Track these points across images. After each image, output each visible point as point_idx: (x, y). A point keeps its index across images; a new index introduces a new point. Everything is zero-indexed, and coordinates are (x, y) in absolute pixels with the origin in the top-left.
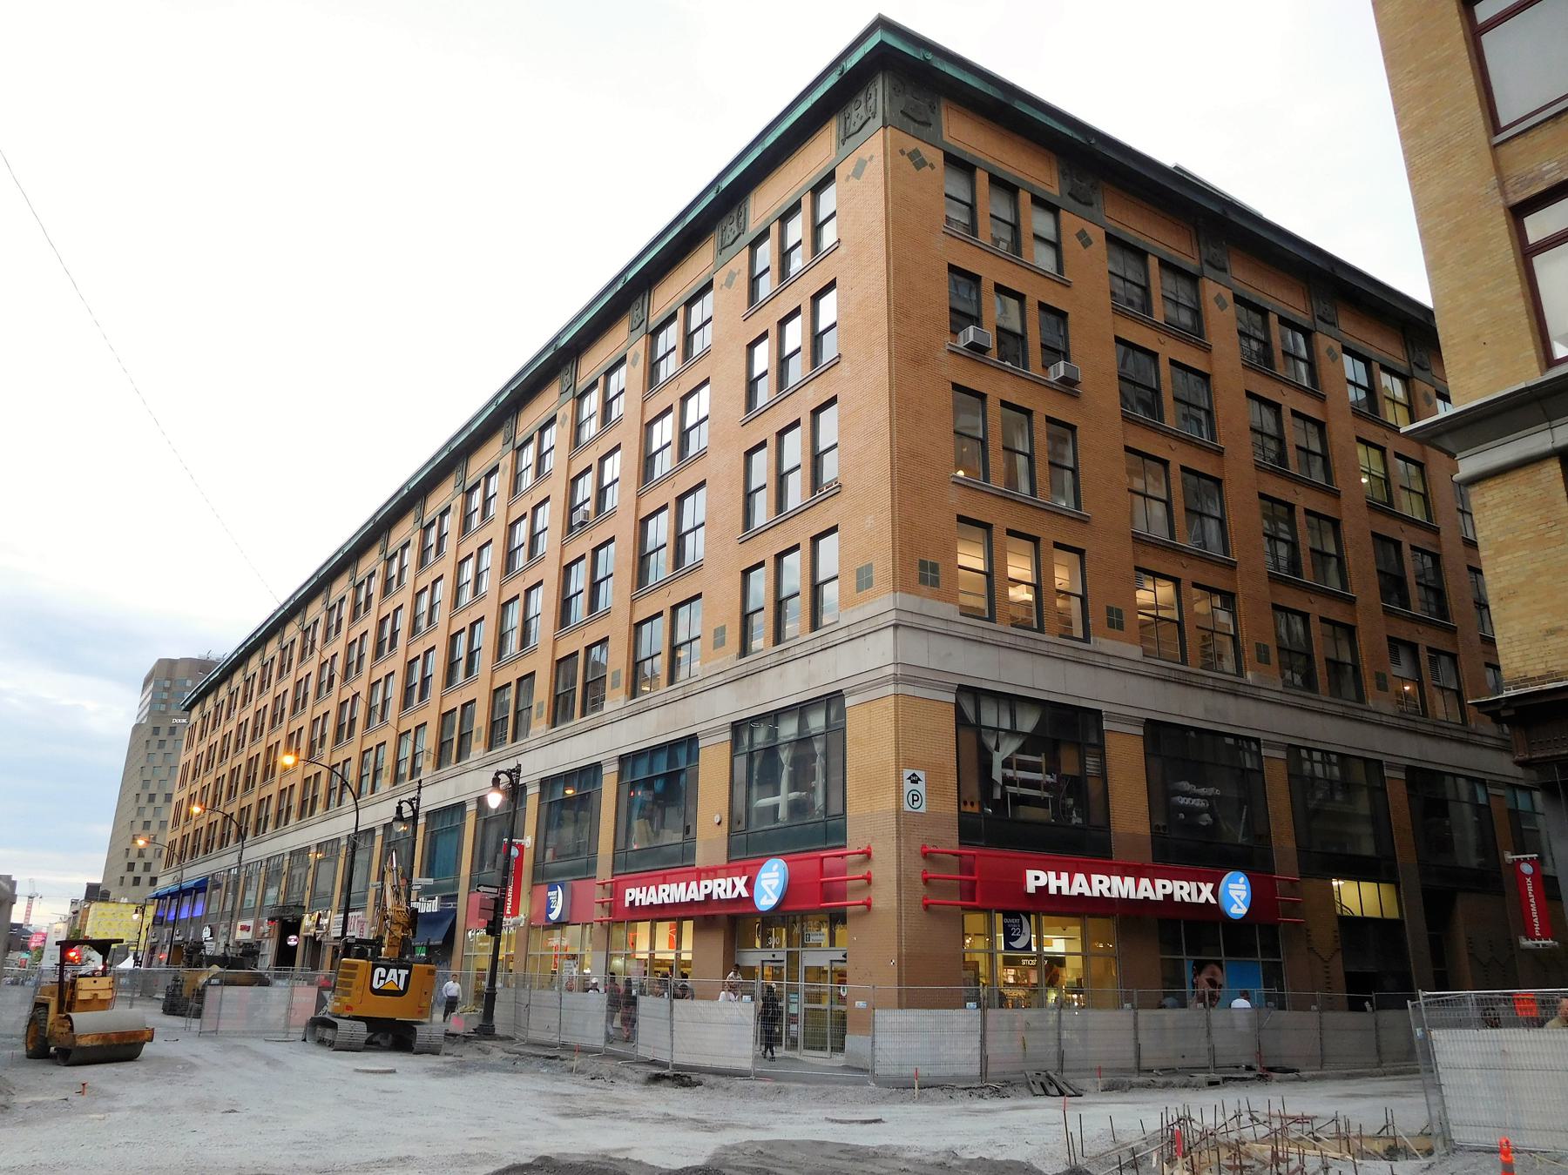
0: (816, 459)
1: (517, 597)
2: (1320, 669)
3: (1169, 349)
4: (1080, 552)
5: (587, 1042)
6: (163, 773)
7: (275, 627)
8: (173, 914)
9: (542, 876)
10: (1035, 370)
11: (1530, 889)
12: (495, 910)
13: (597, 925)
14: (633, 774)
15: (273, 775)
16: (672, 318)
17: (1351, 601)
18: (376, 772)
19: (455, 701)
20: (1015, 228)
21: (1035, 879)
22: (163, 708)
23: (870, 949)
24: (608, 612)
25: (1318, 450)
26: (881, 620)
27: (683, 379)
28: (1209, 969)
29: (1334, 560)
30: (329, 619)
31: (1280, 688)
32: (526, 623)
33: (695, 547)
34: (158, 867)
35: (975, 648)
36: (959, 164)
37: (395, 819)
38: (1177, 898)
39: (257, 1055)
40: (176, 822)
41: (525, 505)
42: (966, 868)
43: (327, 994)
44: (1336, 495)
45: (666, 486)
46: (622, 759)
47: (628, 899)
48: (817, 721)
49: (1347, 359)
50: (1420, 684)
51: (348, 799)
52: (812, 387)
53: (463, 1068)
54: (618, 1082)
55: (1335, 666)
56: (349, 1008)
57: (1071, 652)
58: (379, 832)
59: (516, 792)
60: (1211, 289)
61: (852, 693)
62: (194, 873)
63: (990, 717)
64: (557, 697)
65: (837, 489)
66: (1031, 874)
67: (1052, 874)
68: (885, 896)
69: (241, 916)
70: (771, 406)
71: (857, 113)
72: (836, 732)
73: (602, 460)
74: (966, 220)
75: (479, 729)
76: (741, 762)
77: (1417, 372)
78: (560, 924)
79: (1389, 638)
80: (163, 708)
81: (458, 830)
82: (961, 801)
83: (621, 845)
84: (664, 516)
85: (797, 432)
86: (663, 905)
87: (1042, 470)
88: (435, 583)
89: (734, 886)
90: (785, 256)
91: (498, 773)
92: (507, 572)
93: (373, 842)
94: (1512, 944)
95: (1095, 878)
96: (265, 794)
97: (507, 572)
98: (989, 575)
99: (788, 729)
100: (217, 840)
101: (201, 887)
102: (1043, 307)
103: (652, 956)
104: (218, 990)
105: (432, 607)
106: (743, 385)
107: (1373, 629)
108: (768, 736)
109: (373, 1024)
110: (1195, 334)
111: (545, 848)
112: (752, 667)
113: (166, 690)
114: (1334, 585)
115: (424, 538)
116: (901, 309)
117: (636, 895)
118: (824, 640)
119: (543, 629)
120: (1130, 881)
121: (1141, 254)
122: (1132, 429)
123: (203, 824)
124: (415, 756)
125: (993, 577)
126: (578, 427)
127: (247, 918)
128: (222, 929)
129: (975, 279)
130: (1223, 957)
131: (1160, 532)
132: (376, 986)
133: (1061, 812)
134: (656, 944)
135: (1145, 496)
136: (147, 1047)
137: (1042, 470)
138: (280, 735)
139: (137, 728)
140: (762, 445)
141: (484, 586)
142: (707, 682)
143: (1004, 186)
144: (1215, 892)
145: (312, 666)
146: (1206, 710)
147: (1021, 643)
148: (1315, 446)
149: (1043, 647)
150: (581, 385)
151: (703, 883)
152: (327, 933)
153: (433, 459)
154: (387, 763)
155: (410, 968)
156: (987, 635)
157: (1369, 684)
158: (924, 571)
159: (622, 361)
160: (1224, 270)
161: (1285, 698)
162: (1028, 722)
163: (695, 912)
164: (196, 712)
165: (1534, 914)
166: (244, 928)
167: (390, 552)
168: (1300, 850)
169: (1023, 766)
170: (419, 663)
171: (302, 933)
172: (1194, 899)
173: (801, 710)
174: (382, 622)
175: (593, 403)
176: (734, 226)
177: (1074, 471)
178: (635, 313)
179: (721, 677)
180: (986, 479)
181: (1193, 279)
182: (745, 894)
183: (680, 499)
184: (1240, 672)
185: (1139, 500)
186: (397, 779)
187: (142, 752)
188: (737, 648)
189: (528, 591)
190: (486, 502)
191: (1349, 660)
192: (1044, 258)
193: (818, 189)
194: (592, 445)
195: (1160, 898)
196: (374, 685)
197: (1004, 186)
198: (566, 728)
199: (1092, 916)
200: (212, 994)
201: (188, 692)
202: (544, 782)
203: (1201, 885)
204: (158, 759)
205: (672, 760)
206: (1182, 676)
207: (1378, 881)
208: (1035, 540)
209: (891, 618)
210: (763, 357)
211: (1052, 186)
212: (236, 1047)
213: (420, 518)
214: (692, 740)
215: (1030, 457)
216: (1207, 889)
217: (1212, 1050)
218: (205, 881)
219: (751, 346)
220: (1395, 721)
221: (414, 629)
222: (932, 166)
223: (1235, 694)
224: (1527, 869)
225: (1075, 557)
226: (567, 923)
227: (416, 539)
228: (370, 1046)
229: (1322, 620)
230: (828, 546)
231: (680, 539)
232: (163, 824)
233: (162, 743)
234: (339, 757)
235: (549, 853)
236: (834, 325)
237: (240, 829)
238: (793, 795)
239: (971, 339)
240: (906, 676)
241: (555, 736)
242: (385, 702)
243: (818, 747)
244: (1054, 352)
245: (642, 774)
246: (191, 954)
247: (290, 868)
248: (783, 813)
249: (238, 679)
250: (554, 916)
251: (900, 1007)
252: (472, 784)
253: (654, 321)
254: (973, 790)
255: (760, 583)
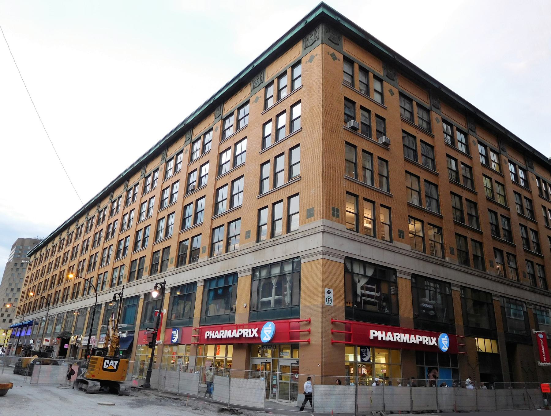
0: (290, 167)
1: (164, 217)
2: (471, 258)
3: (420, 136)
4: (389, 208)
5: (189, 393)
6: (17, 281)
7: (75, 219)
8: (18, 334)
9: (170, 325)
10: (374, 138)
11: (542, 344)
12: (153, 338)
13: (192, 345)
14: (210, 287)
15: (62, 282)
16: (232, 114)
17: (481, 233)
18: (104, 283)
19: (137, 256)
20: (367, 86)
21: (374, 334)
22: (19, 256)
23: (311, 358)
24: (201, 224)
25: (469, 177)
26: (317, 229)
27: (235, 137)
28: (433, 371)
29: (475, 218)
30: (77, 232)
31: (458, 264)
32: (167, 227)
33: (238, 201)
34: (13, 316)
35: (352, 242)
36: (348, 60)
37: (113, 301)
38: (424, 343)
39: (55, 395)
40: (22, 299)
41: (169, 183)
42: (347, 329)
43: (82, 369)
44: (476, 194)
45: (228, 177)
46: (205, 281)
47: (206, 336)
48: (288, 268)
49: (479, 146)
50: (503, 265)
51: (92, 292)
52: (289, 140)
53: (140, 404)
54: (206, 411)
55: (475, 257)
56: (93, 376)
57: (386, 246)
58: (104, 306)
59: (162, 292)
60: (435, 116)
61: (304, 258)
62: (28, 319)
63: (357, 269)
64: (179, 256)
65: (299, 179)
66: (372, 332)
67: (380, 332)
68: (316, 338)
69: (46, 336)
70: (272, 147)
71: (310, 39)
72: (297, 271)
73: (201, 166)
74: (350, 82)
75: (147, 267)
76: (255, 283)
77: (502, 152)
78: (177, 344)
79: (494, 248)
80: (19, 256)
81: (136, 306)
82: (346, 302)
83: (204, 314)
84: (191, 206)
85: (269, 164)
86: (221, 339)
87: (376, 177)
88: (131, 211)
89: (252, 332)
90: (279, 91)
91: (157, 284)
92: (161, 208)
93: (101, 309)
94: (535, 364)
95: (395, 334)
96: (58, 289)
97: (161, 208)
98: (357, 215)
99: (276, 271)
100: (38, 307)
101: (30, 324)
102: (377, 116)
103: (226, 359)
104: (39, 367)
105: (129, 221)
106: (261, 139)
107: (489, 246)
108: (267, 273)
109: (103, 383)
110: (429, 131)
111: (172, 314)
112: (261, 246)
113: (20, 250)
114: (475, 227)
115: (166, 166)
116: (327, 111)
117: (210, 334)
118: (292, 237)
119: (174, 230)
120: (407, 336)
121: (410, 100)
122: (407, 164)
123: (33, 300)
124: (119, 277)
125: (358, 215)
126: (192, 154)
127: (48, 337)
128: (38, 340)
129: (354, 103)
130: (438, 366)
131: (416, 202)
132: (105, 367)
133: (381, 308)
134: (223, 354)
135: (411, 189)
136: (10, 390)
137: (376, 177)
138: (66, 267)
139: (8, 263)
140: (268, 161)
141: (151, 213)
142: (242, 252)
143: (365, 71)
144: (437, 341)
145: (80, 241)
146: (433, 271)
147: (368, 241)
148: (468, 175)
149: (376, 243)
150: (194, 139)
151: (239, 330)
152: (80, 344)
153: (133, 165)
154: (108, 279)
155: (119, 360)
156: (356, 238)
157: (487, 264)
158: (334, 212)
159: (211, 130)
160: (438, 109)
161: (459, 268)
162: (370, 273)
163: (235, 342)
164: (33, 257)
165: (544, 353)
166: (46, 340)
167: (100, 209)
168: (465, 326)
169: (368, 289)
170: (123, 241)
171: (70, 343)
172: (430, 344)
173: (281, 263)
174: (109, 226)
175: (171, 164)
176: (259, 80)
177: (387, 178)
178: (217, 112)
179: (248, 250)
180: (356, 177)
181: (428, 111)
182: (257, 335)
183: (233, 182)
184: (444, 257)
185: (410, 190)
186: (112, 285)
187: (10, 272)
188: (255, 239)
189: (169, 215)
190: (153, 181)
191: (480, 255)
192: (377, 98)
193: (293, 67)
194: (200, 160)
195: (418, 343)
196: (91, 256)
197: (365, 71)
198: (182, 268)
199: (392, 349)
200: (36, 368)
201: (29, 250)
202: (172, 289)
203: (432, 338)
204: (16, 275)
205: (226, 282)
206: (425, 258)
207: (491, 339)
208: (373, 203)
209: (322, 228)
210: (269, 129)
211: (381, 73)
212: (46, 391)
213: (126, 187)
214: (235, 274)
215: (372, 171)
216: (434, 339)
217: (438, 403)
218: (32, 322)
219: (265, 124)
220: (496, 279)
221: (122, 229)
222: (339, 60)
223: (443, 266)
224: (541, 336)
225: (387, 210)
226: (180, 344)
227: (124, 194)
228: (101, 391)
229: (472, 240)
230: (295, 201)
231: (232, 197)
232: (16, 300)
233: (18, 269)
234: (88, 277)
235: (173, 316)
236: (299, 117)
237: (48, 302)
238: (277, 297)
239: (352, 125)
240: (327, 251)
241: (178, 271)
242: (108, 256)
243: (288, 278)
244: (381, 133)
245: (213, 286)
246: (28, 351)
247: (67, 318)
248: (272, 304)
249: (50, 246)
250: (174, 341)
251: (322, 384)
252: (145, 286)
253: (225, 115)
254: (350, 298)
255: (265, 215)
